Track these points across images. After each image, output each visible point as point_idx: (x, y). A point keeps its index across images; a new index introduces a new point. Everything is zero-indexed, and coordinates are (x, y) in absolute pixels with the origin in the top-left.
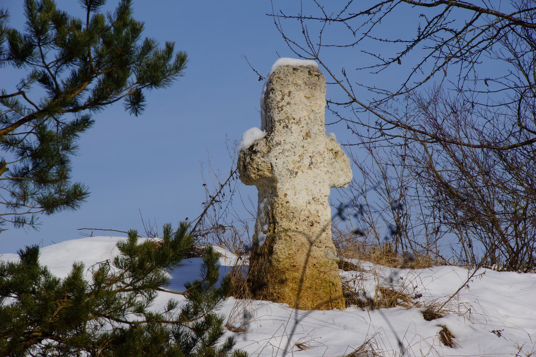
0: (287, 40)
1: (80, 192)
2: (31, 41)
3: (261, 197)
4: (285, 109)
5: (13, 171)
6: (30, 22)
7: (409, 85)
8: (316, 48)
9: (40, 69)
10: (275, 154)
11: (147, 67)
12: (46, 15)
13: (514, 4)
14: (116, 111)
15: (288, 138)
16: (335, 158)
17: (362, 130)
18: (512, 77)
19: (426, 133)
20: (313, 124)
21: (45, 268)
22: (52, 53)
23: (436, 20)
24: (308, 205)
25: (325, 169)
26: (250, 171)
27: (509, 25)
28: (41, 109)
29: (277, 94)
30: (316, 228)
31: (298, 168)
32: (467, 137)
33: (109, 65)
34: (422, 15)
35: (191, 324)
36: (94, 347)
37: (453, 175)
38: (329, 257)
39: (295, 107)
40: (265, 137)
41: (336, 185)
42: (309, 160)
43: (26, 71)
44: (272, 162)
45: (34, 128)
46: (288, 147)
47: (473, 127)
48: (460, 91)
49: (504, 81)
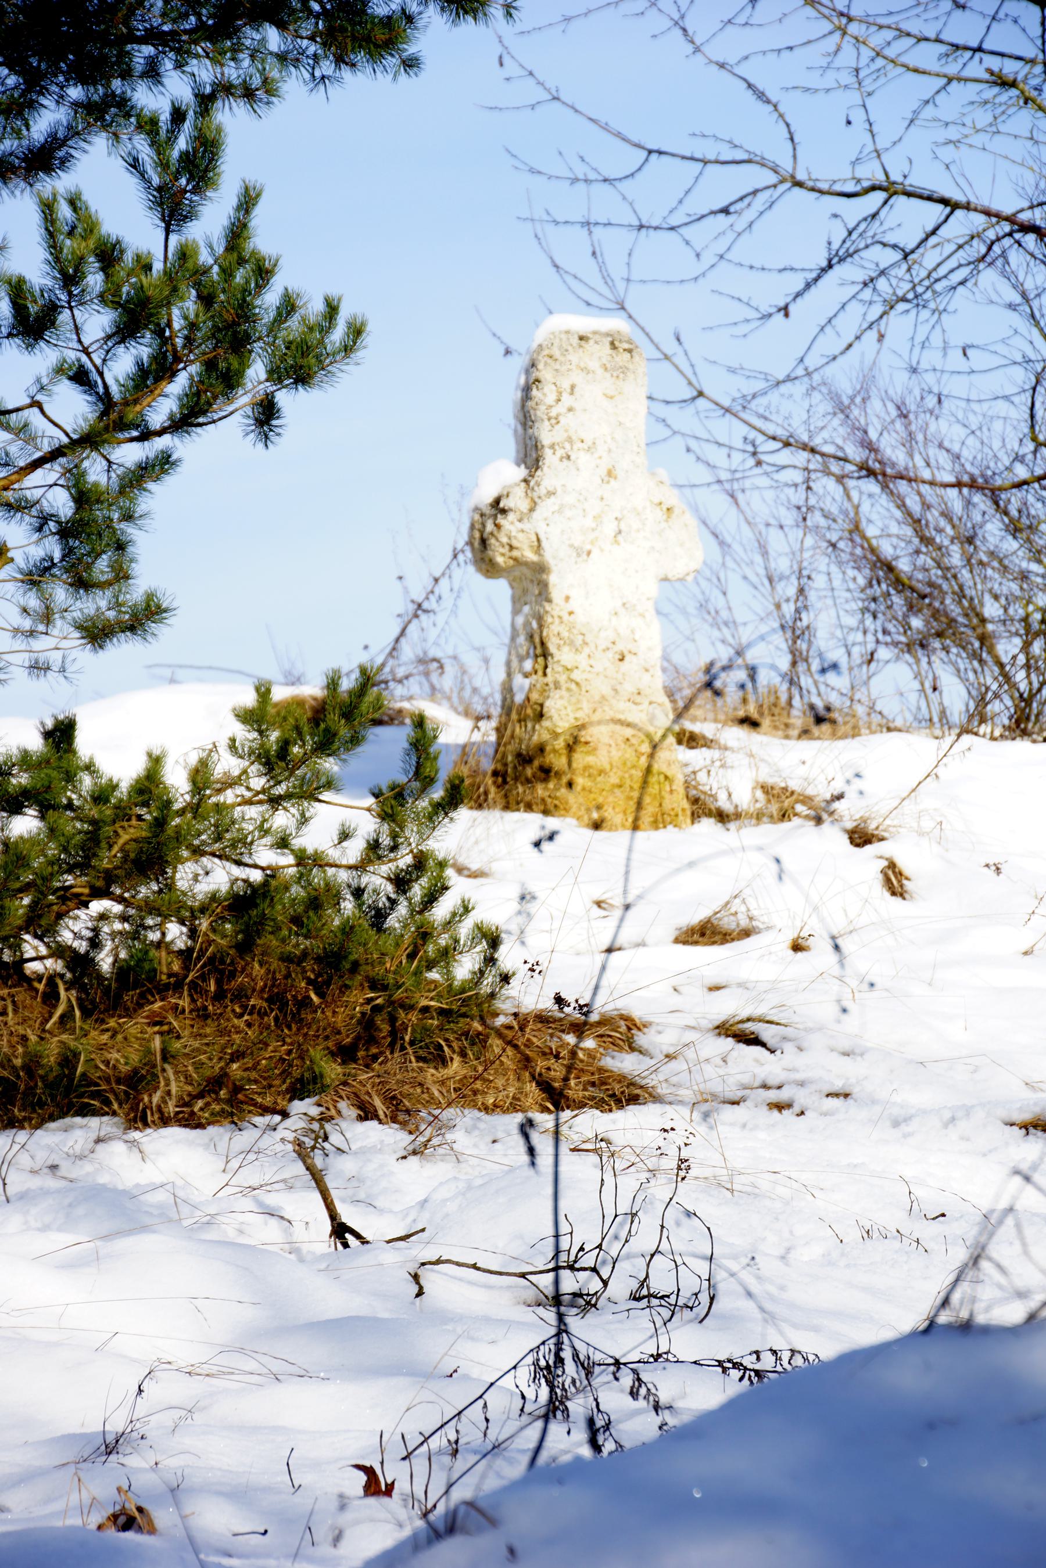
0: (569, 279)
1: (158, 607)
2: (53, 298)
3: (517, 602)
4: (562, 419)
5: (23, 565)
6: (50, 258)
7: (811, 362)
8: (621, 286)
9: (72, 355)
11: (288, 348)
12: (84, 244)
13: (1020, 191)
14: (228, 432)
17: (717, 456)
18: (1019, 342)
19: (845, 460)
21: (91, 759)
22: (97, 322)
23: (863, 226)
27: (1010, 234)
28: (75, 437)
31: (592, 543)
32: (928, 465)
33: (210, 345)
34: (835, 216)
35: (385, 869)
36: (194, 917)
37: (903, 544)
40: (525, 481)
41: (670, 576)
43: (44, 358)
45: (63, 474)
47: (941, 446)
48: (914, 370)
49: (1001, 348)
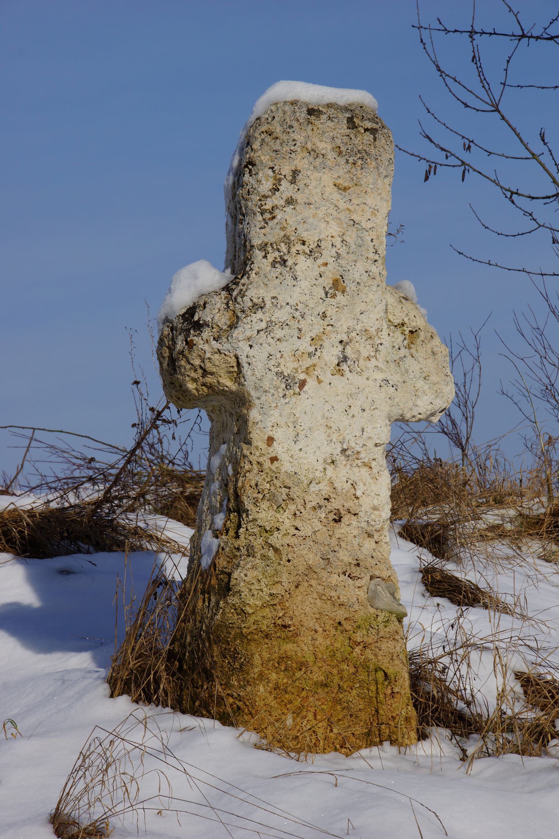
4: (279, 215)
8: (496, 89)
10: (248, 334)
15: (286, 292)
20: (352, 257)
24: (330, 468)
25: (380, 376)
26: (183, 375)
29: (260, 174)
30: (348, 529)
31: (307, 371)
38: (380, 604)
39: (307, 213)
40: (227, 288)
41: (408, 416)
42: (337, 351)
44: (239, 353)
46: (282, 315)
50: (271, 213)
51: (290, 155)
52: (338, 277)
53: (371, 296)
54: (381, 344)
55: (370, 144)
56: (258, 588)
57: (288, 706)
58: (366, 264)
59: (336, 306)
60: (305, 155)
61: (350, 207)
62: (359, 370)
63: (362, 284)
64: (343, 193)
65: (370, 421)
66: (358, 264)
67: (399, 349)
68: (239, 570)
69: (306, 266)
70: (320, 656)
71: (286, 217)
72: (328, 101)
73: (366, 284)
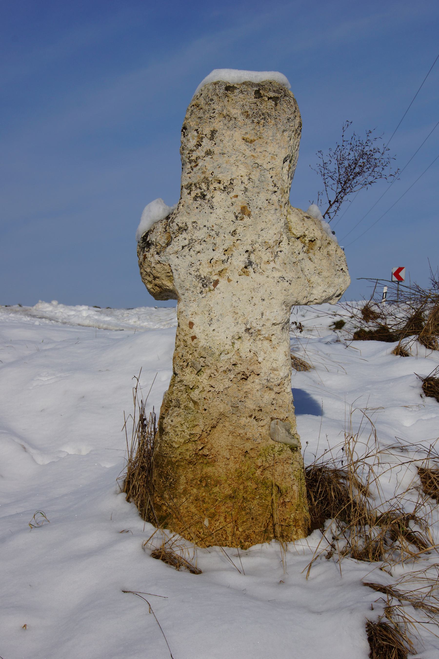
4: (201, 163)
10: (176, 249)
16: (307, 252)
20: (256, 190)
25: (277, 274)
29: (189, 136)
31: (220, 273)
39: (221, 160)
42: (244, 258)
46: (200, 234)
50: (195, 162)
51: (210, 120)
52: (245, 205)
53: (269, 217)
54: (281, 251)
55: (272, 108)
56: (181, 430)
57: (205, 512)
58: (267, 194)
59: (243, 226)
60: (221, 119)
61: (254, 154)
62: (261, 271)
63: (263, 209)
64: (250, 144)
65: (268, 307)
66: (261, 195)
67: (299, 254)
68: (168, 417)
69: (221, 198)
70: (230, 476)
71: (206, 164)
72: (243, 82)
73: (266, 209)
